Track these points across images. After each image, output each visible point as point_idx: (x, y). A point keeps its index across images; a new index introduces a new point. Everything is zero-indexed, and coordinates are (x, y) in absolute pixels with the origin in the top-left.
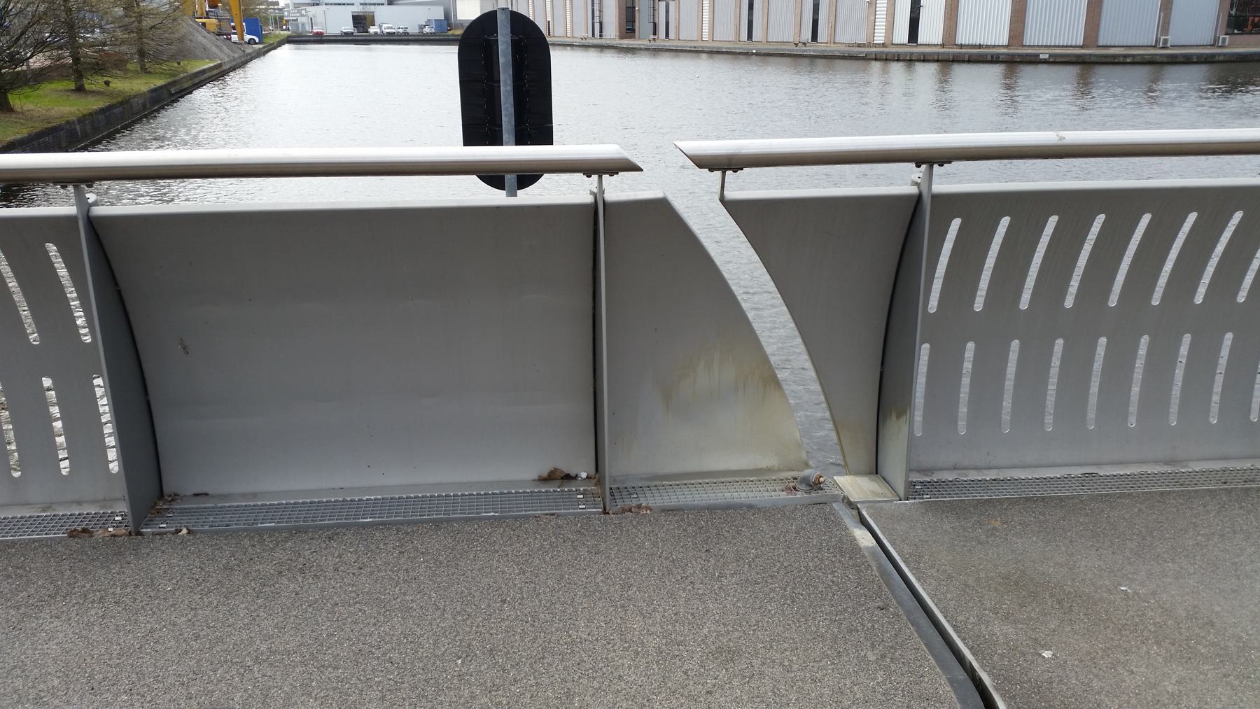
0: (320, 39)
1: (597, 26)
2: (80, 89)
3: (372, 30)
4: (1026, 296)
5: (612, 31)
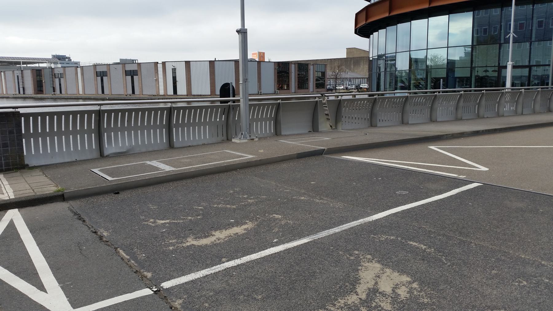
1: (21, 90)
4: (33, 151)
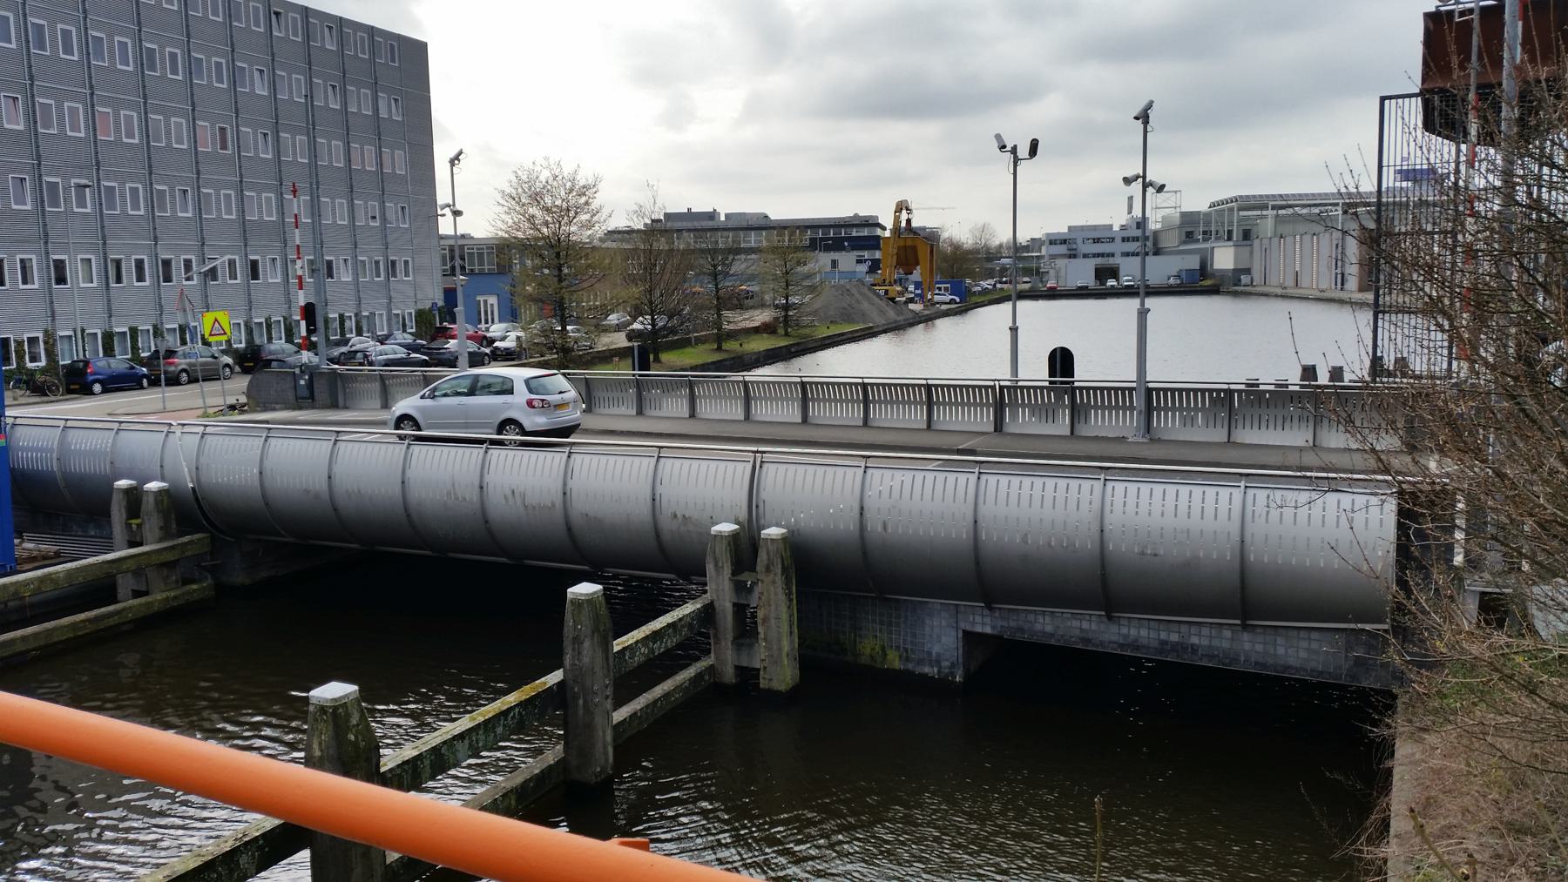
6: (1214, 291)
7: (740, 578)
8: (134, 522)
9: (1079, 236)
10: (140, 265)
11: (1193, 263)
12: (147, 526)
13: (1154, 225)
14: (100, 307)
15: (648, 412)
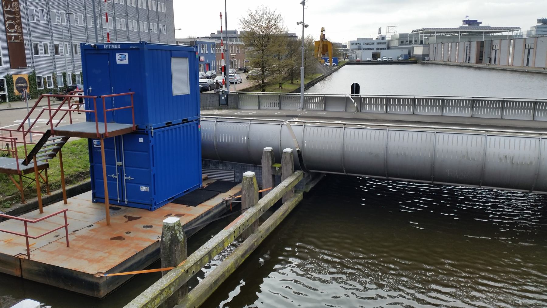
0: (359, 63)
1: (468, 58)
2: (292, 83)
3: (379, 59)
5: (473, 60)
6: (415, 62)
7: (274, 166)
8: (277, 166)
9: (362, 42)
10: (45, 46)
11: (406, 52)
12: (284, 168)
13: (388, 38)
14: (51, 65)
15: (262, 107)
